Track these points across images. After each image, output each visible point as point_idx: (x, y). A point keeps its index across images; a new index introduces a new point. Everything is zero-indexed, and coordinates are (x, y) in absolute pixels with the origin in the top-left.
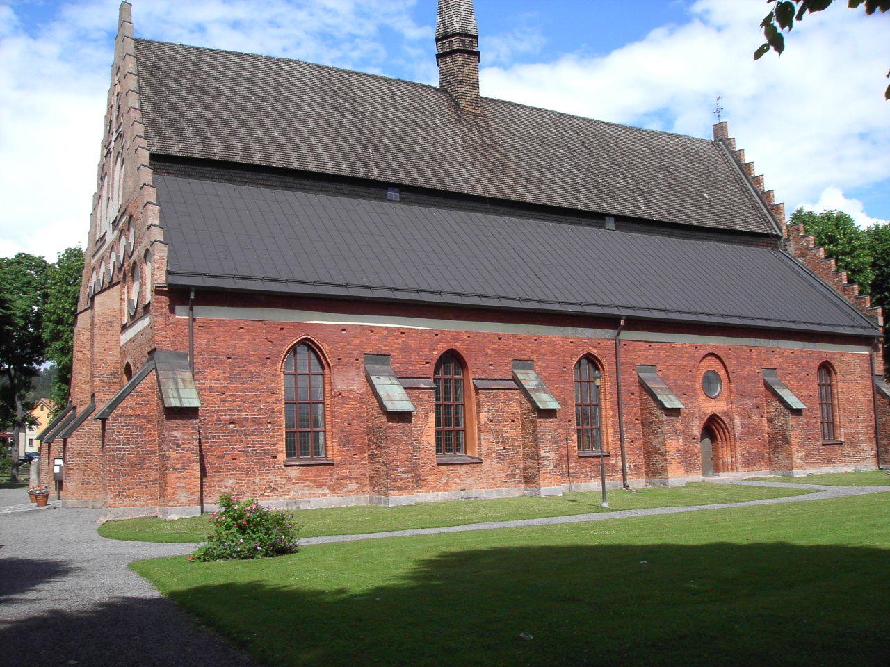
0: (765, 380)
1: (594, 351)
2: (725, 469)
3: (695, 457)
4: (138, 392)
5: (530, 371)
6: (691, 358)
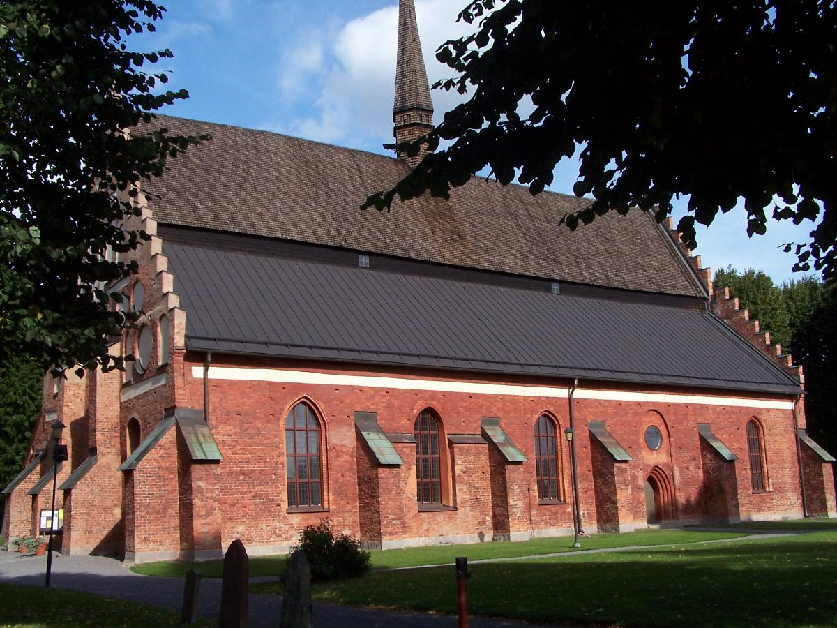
0: (700, 434)
1: (551, 409)
3: (640, 505)
5: (497, 428)
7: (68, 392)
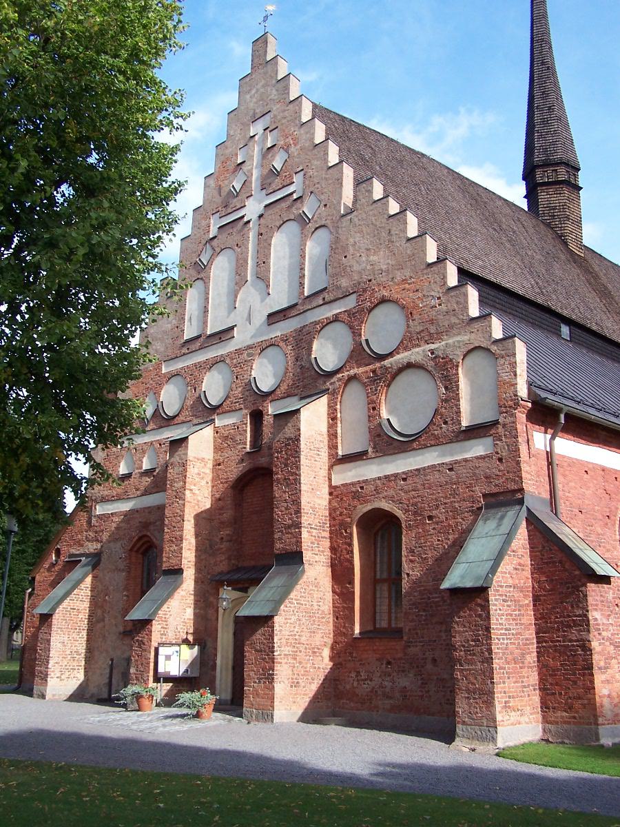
7: (192, 470)
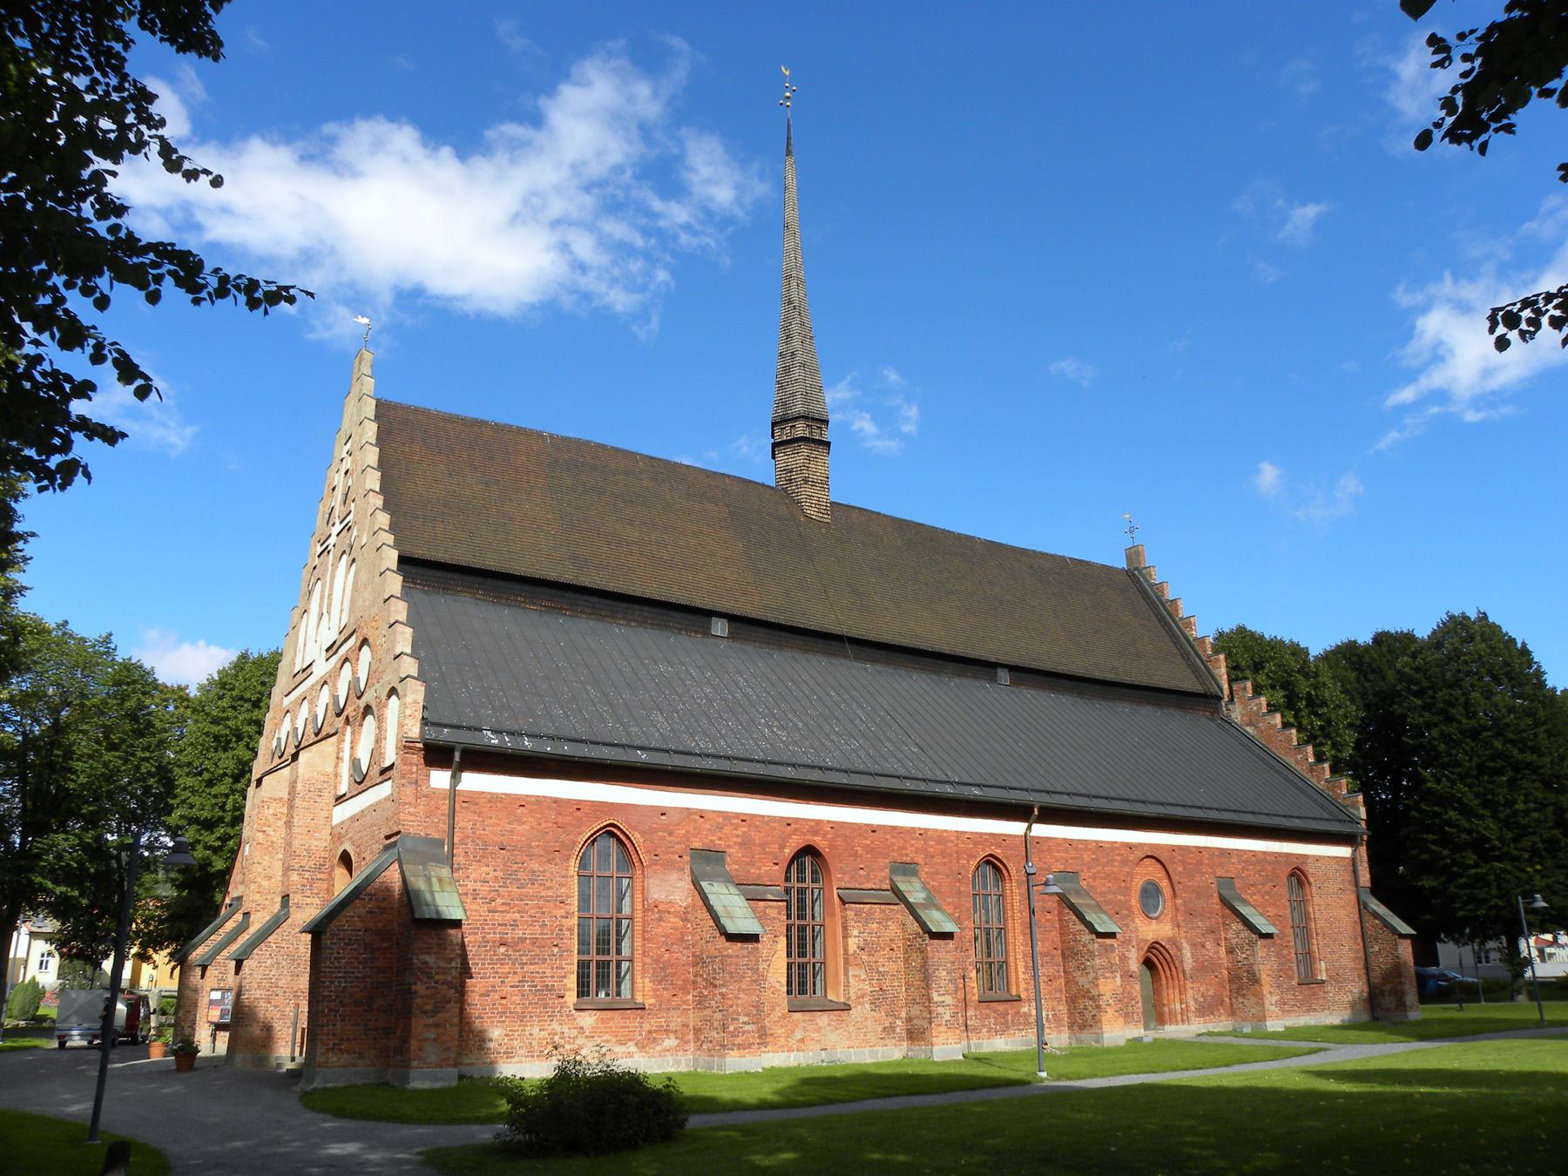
1: (998, 852)
2: (1173, 1021)
4: (372, 895)
5: (913, 879)
6: (1125, 862)
